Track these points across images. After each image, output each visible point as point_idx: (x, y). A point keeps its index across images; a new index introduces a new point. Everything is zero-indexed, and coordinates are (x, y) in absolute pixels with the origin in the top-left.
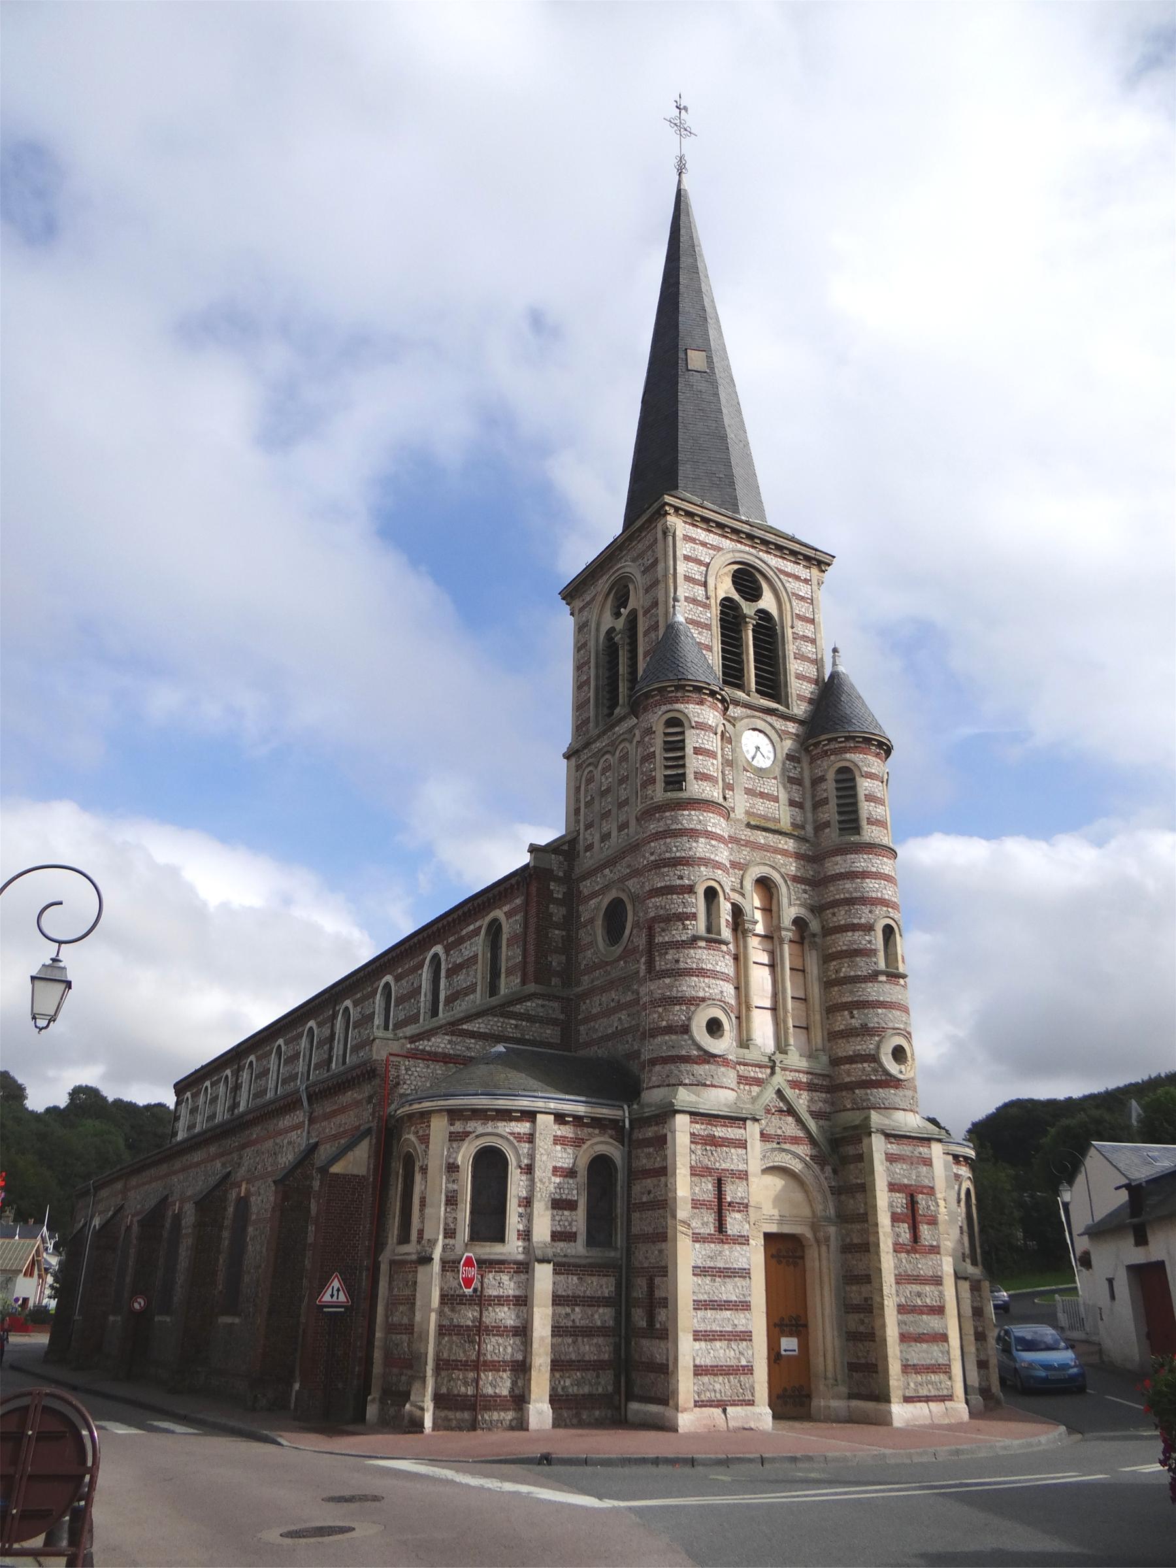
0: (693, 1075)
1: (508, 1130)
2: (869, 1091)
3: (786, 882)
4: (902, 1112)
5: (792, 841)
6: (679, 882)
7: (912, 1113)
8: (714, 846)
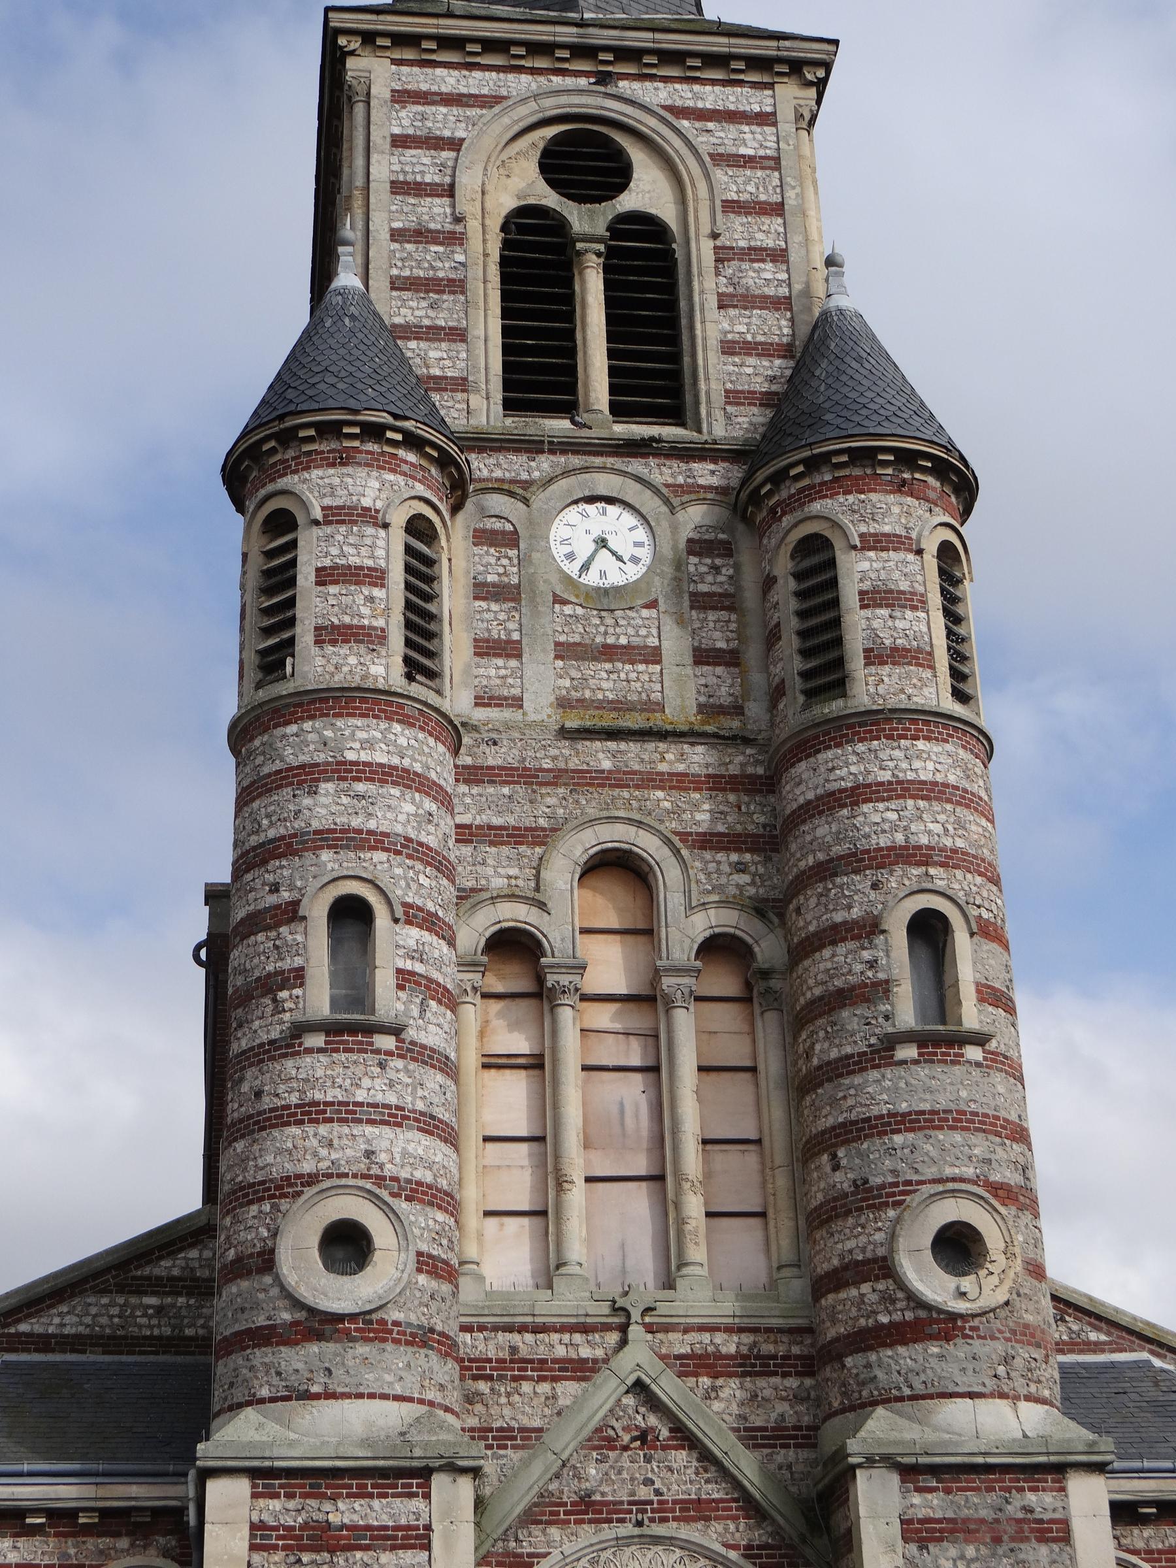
0: (279, 1374)
2: (873, 1357)
3: (677, 852)
5: (700, 749)
6: (272, 900)
8: (360, 797)
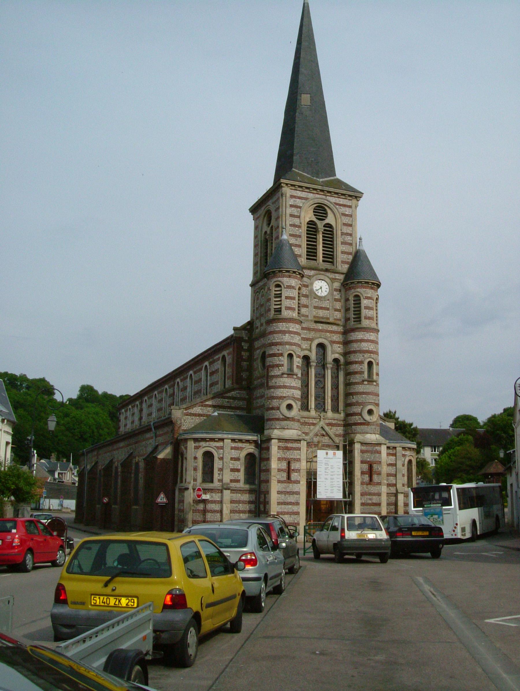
1: (214, 445)
2: (357, 427)
4: (369, 434)
6: (278, 352)
7: (374, 435)
8: (292, 337)
